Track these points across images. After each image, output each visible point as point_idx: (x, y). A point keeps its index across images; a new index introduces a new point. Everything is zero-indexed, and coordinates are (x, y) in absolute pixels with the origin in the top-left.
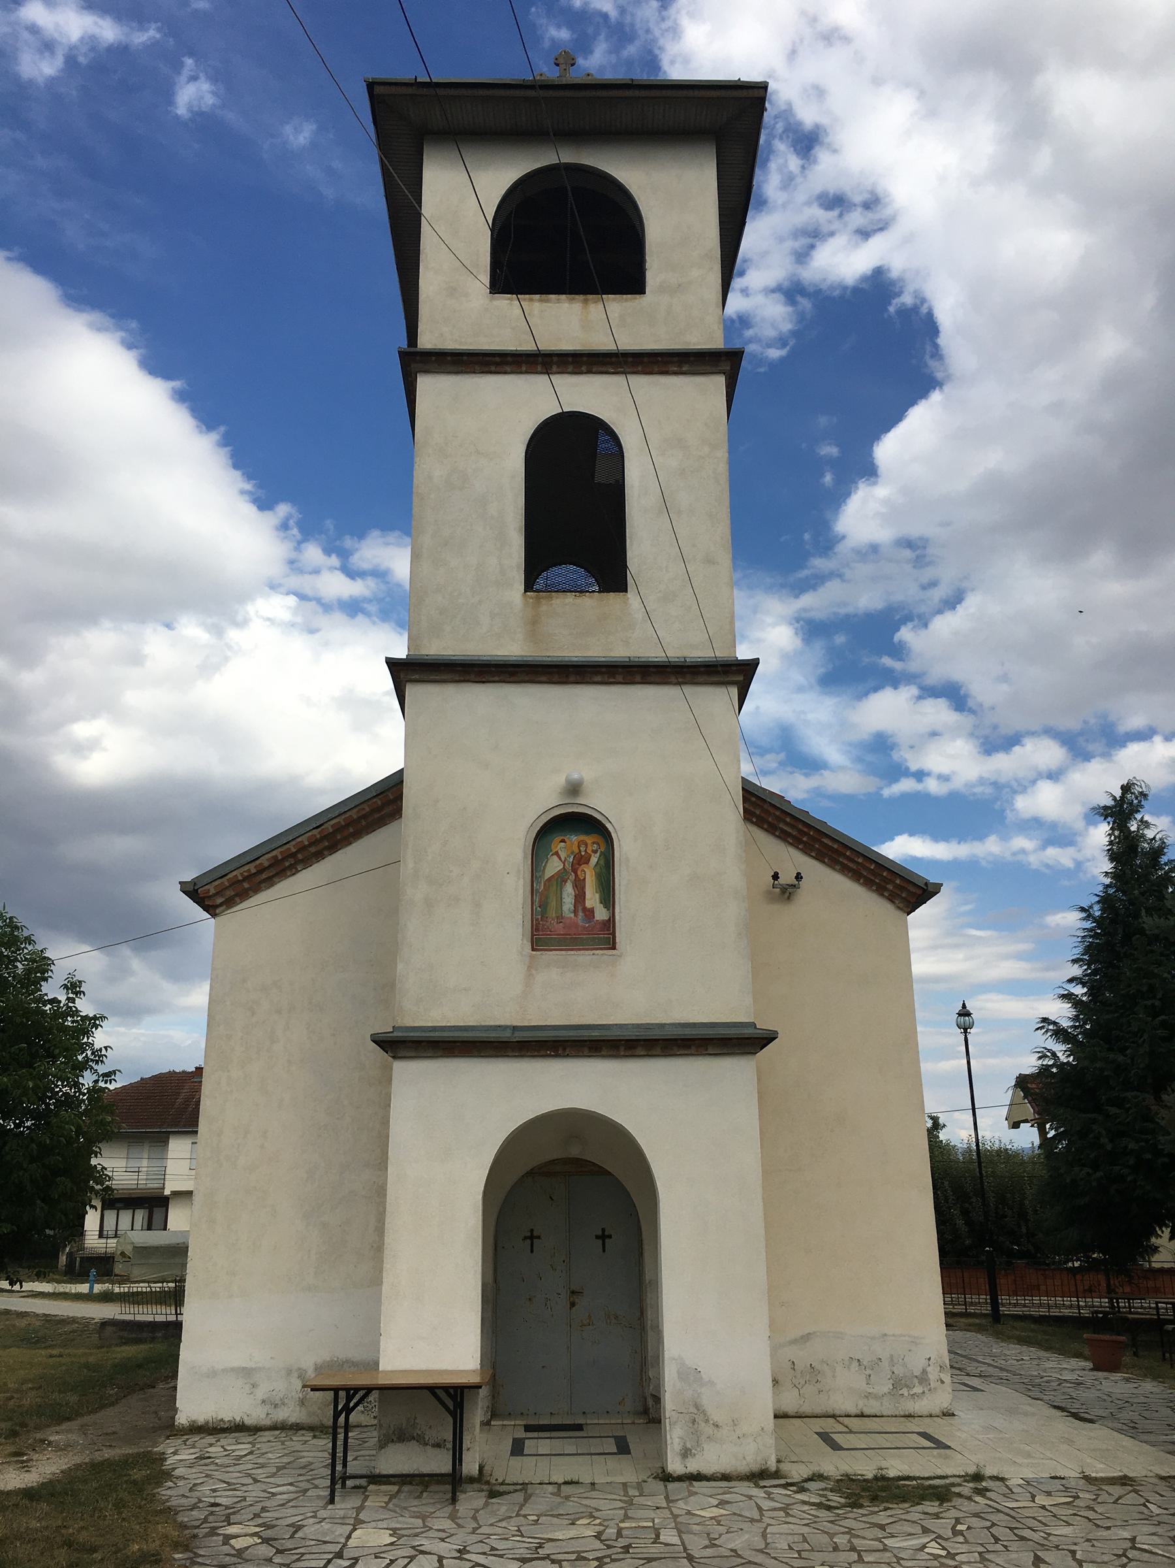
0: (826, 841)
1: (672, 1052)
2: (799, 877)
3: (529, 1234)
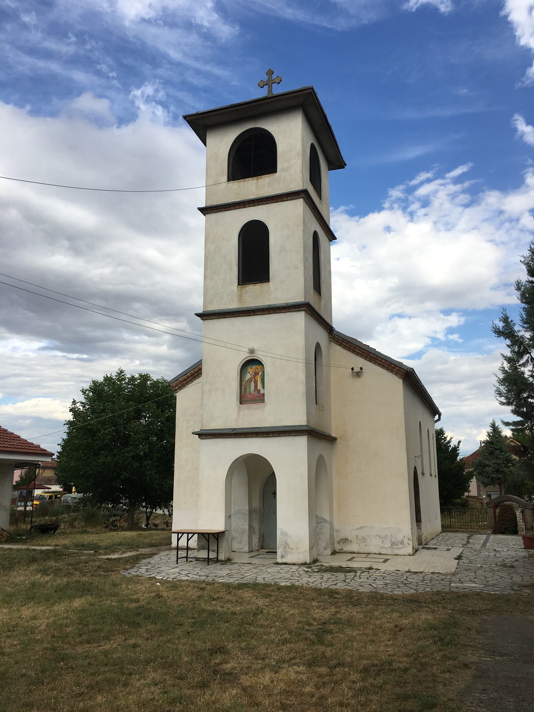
0: (371, 355)
1: (281, 435)
2: (361, 369)
3: (273, 492)
